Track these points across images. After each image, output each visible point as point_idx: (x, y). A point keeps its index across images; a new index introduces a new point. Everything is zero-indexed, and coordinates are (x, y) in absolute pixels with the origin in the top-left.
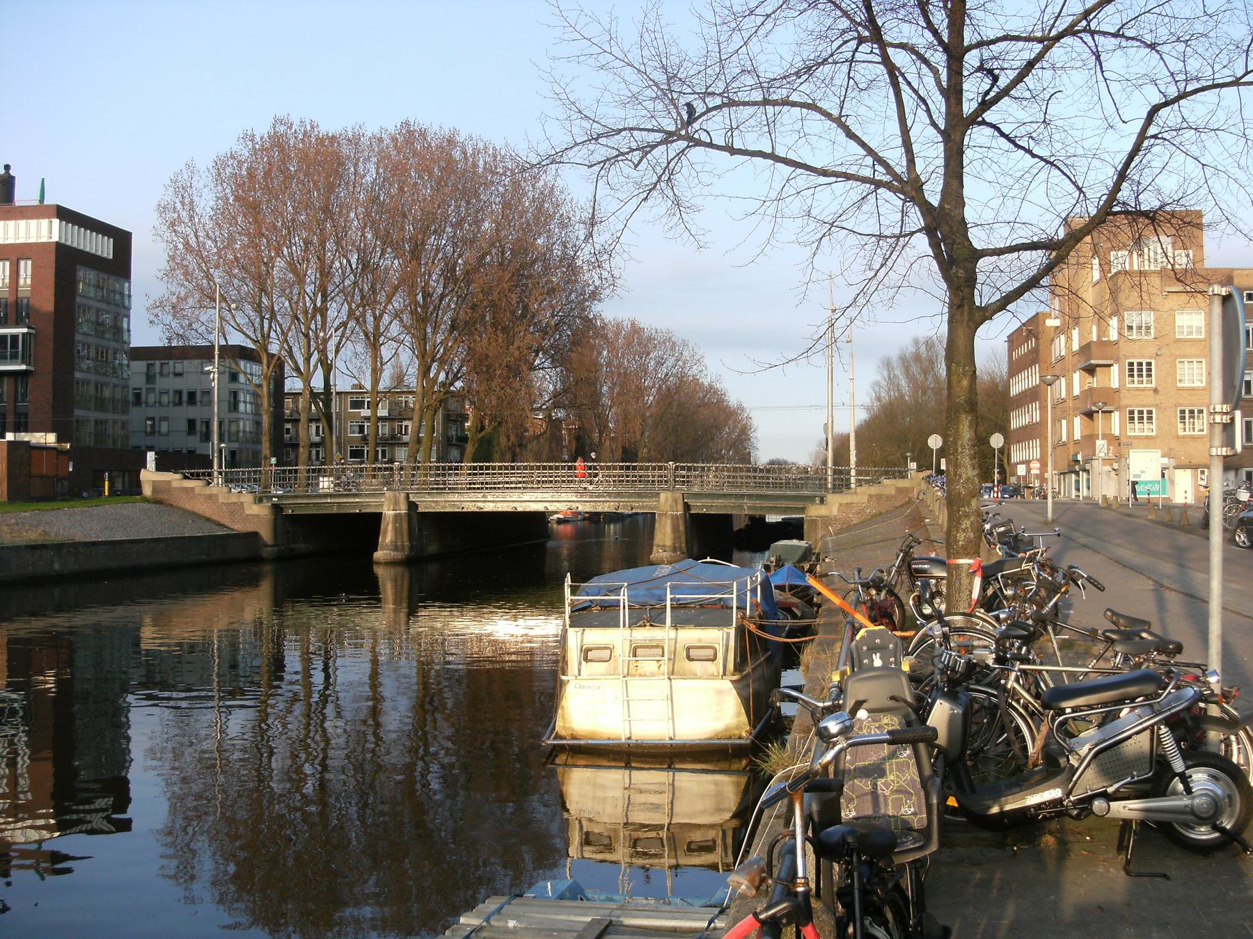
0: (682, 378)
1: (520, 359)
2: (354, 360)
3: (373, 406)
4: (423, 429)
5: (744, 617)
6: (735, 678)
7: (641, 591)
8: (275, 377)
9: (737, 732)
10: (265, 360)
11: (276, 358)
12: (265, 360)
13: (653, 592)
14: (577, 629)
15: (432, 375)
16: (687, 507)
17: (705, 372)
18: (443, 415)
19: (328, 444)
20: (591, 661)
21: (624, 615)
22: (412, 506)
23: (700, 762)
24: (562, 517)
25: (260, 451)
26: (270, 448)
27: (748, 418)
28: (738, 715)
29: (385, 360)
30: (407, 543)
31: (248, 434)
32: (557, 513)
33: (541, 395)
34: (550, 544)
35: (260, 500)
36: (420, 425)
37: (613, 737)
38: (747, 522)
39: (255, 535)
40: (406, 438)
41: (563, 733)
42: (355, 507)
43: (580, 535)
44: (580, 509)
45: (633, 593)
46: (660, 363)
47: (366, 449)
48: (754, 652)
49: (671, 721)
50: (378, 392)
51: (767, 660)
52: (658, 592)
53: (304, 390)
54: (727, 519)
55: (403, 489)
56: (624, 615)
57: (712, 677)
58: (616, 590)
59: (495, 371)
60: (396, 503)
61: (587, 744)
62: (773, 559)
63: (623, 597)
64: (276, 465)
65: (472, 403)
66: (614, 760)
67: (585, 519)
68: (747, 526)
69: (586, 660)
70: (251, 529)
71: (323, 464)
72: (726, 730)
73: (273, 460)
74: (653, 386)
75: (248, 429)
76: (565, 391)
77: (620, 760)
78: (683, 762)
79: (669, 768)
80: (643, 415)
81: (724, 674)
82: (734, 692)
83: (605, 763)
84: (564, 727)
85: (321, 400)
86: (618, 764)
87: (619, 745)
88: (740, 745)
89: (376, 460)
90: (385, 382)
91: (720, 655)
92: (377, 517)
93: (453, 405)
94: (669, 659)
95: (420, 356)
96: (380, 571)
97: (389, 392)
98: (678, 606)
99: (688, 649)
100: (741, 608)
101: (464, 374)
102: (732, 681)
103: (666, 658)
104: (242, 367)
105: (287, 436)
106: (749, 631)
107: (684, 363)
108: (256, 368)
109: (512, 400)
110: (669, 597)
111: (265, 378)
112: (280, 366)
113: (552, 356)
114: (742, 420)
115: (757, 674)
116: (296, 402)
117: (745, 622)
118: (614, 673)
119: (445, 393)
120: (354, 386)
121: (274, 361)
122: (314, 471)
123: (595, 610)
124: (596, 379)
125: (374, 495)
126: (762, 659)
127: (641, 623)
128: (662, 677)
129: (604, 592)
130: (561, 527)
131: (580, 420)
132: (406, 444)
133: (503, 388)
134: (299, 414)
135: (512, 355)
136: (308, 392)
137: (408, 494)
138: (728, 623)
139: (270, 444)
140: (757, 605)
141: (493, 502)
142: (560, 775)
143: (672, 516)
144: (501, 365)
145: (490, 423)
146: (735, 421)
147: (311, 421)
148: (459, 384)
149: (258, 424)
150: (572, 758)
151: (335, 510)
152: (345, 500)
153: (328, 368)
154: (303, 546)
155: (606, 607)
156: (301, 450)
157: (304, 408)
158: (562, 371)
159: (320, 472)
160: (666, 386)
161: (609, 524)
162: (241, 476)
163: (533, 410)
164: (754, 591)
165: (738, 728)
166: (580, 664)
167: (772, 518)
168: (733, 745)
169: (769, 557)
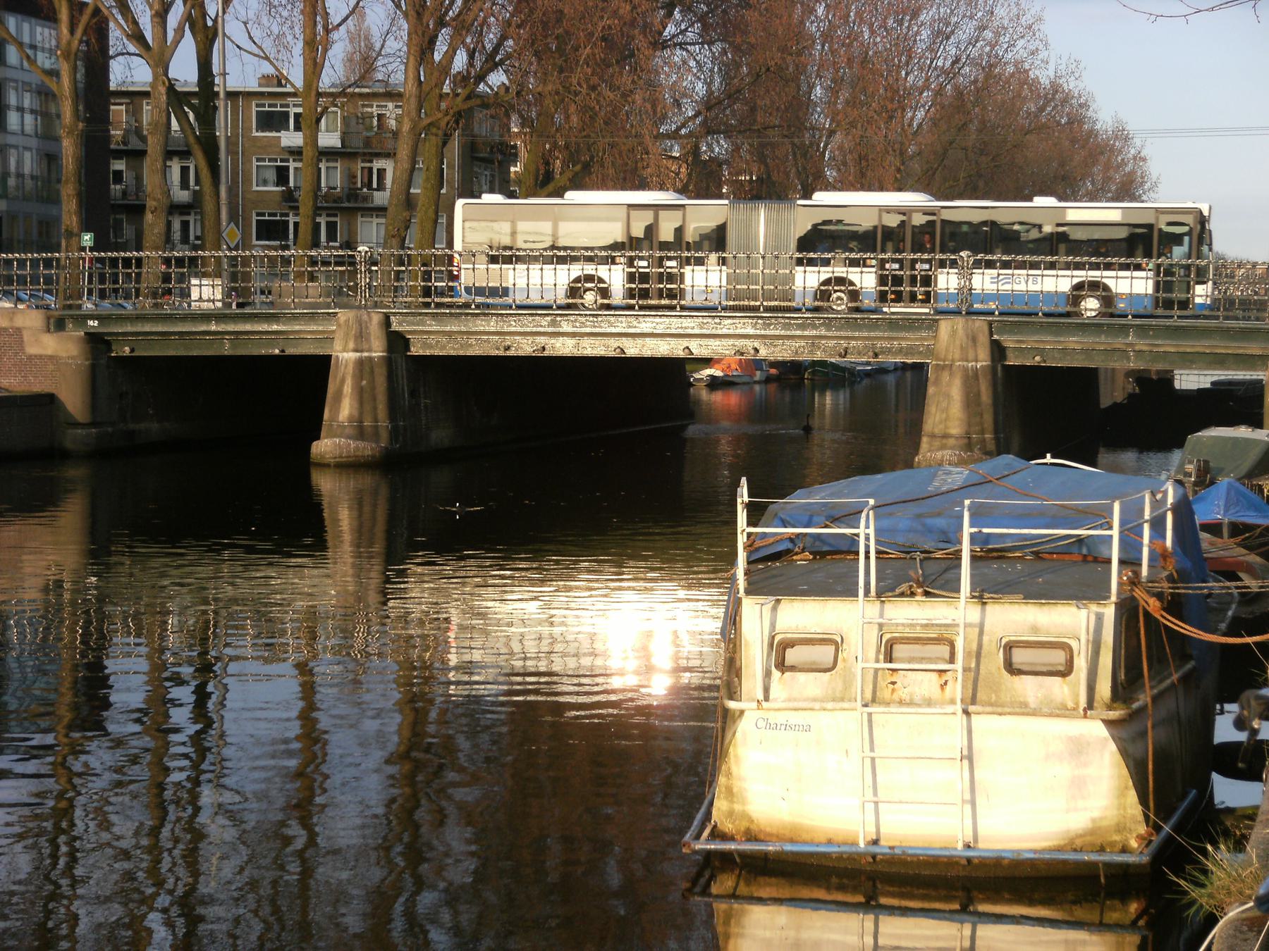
0: (990, 69)
1: (633, 24)
2: (265, 20)
3: (309, 124)
4: (419, 178)
5: (1135, 581)
6: (1114, 714)
7: (903, 520)
8: (87, 53)
9: (1117, 838)
10: (64, 15)
11: (89, 11)
12: (64, 15)
13: (929, 521)
14: (761, 599)
15: (437, 57)
16: (998, 350)
17: (1043, 55)
18: (463, 147)
19: (209, 206)
20: (793, 668)
21: (867, 570)
22: (397, 342)
23: (1031, 902)
24: (719, 373)
25: (58, 219)
26: (79, 213)
27: (1139, 159)
28: (1122, 794)
29: (335, 19)
30: (384, 423)
31: (29, 184)
32: (707, 362)
33: (678, 104)
34: (693, 431)
35: (60, 325)
36: (413, 169)
37: (840, 838)
38: (1132, 387)
39: (48, 401)
40: (380, 198)
41: (728, 827)
42: (271, 343)
43: (759, 412)
44: (763, 353)
45: (886, 523)
46: (942, 35)
47: (292, 219)
48: (1158, 660)
49: (968, 808)
50: (319, 95)
51: (1185, 679)
52: (940, 522)
53: (153, 85)
54: (1084, 379)
55: (376, 305)
56: (867, 570)
57: (1062, 712)
58: (851, 517)
59: (576, 49)
60: (361, 337)
61: (783, 853)
62: (1190, 468)
63: (866, 531)
64: (91, 249)
65: (525, 122)
66: (841, 888)
67: (768, 380)
68: (1131, 396)
69: (782, 666)
70: (38, 386)
71: (196, 248)
72: (1092, 832)
73: (87, 239)
74: (926, 86)
75: (27, 170)
76: (732, 95)
77: (855, 890)
78: (995, 898)
79: (964, 909)
80: (902, 153)
81: (1090, 705)
82: (1112, 747)
83: (820, 894)
84: (731, 814)
85: (192, 107)
86: (850, 898)
87: (854, 857)
88: (1125, 867)
89: (316, 244)
90: (333, 74)
91: (1081, 664)
92: (321, 365)
93: (483, 127)
94: (966, 670)
95: (412, 13)
96: (325, 483)
97: (343, 94)
98: (987, 554)
99: (1009, 647)
100: (1131, 561)
101: (509, 56)
102: (1109, 723)
103: (959, 665)
104: (12, 30)
105: (116, 188)
106: (1147, 614)
107: (997, 34)
108: (42, 34)
109: (615, 112)
110: (967, 530)
111: (66, 55)
112: (99, 30)
113: (702, 19)
114: (1124, 163)
115: (1169, 704)
116: (135, 112)
117: (1139, 594)
118: (840, 698)
119: (469, 97)
120: (266, 79)
121: (85, 18)
122: (180, 262)
123: (802, 560)
124: (800, 69)
125: (312, 317)
126: (1175, 677)
127: (904, 587)
128: (950, 709)
129: (822, 519)
130: (718, 397)
131: (762, 159)
132: (381, 211)
133: (593, 88)
134: (143, 139)
135: (615, 13)
136: (163, 90)
137: (387, 318)
138: (1099, 594)
139: (80, 204)
140: (1164, 555)
141: (573, 335)
142: (718, 921)
143: (965, 369)
144: (591, 34)
145: (565, 164)
146: (1107, 167)
147: (169, 154)
148: (497, 78)
149: (51, 159)
150: (748, 884)
151: (227, 349)
152: (248, 327)
153: (207, 36)
154: (155, 426)
155: (823, 555)
156: (149, 217)
157: (154, 125)
158: (724, 52)
159: (193, 266)
160: (956, 88)
161: (822, 393)
162: (15, 270)
163: (659, 137)
164: (1158, 525)
165: (1120, 828)
166: (768, 674)
167: (1189, 380)
168: (1108, 865)
169: (1182, 461)
